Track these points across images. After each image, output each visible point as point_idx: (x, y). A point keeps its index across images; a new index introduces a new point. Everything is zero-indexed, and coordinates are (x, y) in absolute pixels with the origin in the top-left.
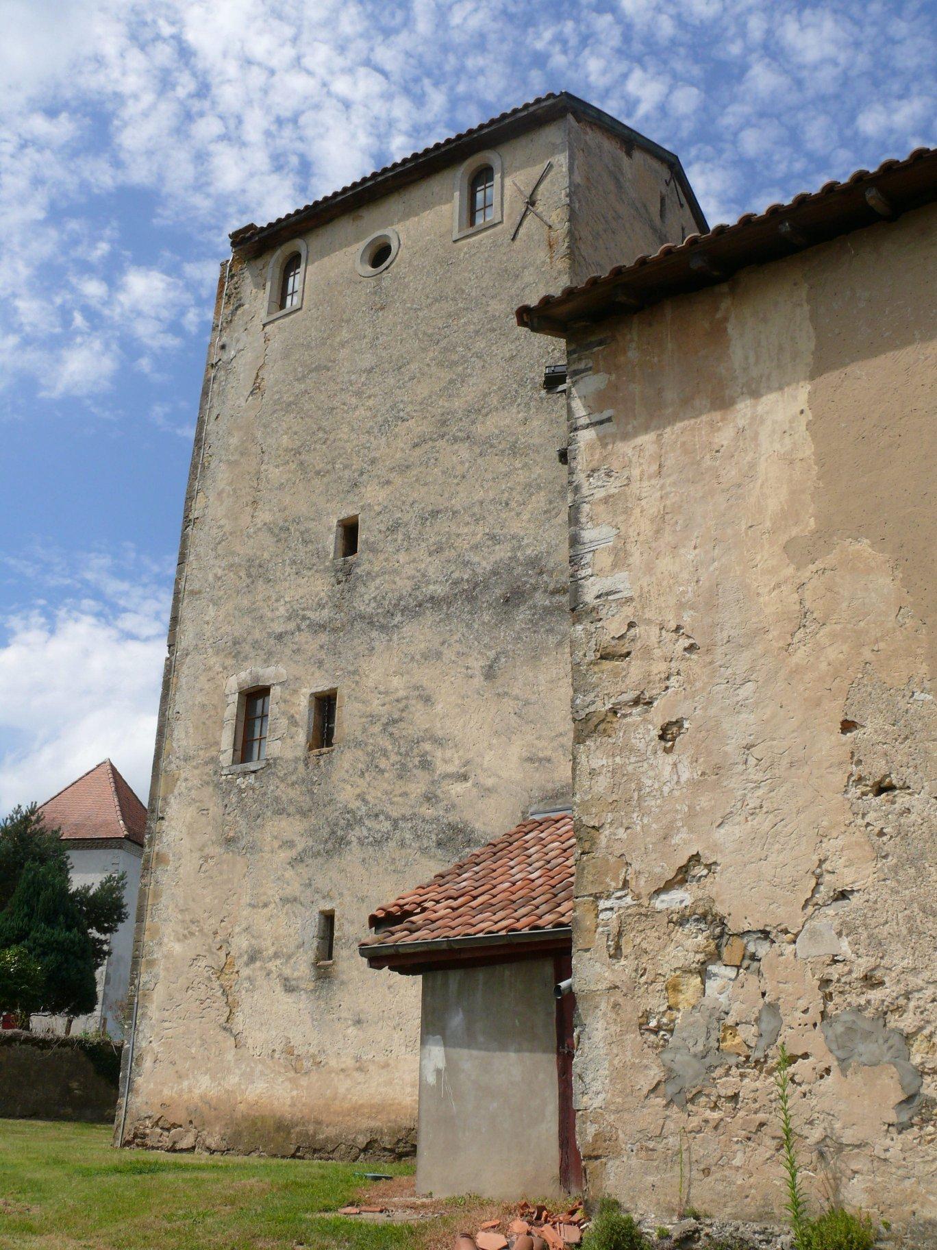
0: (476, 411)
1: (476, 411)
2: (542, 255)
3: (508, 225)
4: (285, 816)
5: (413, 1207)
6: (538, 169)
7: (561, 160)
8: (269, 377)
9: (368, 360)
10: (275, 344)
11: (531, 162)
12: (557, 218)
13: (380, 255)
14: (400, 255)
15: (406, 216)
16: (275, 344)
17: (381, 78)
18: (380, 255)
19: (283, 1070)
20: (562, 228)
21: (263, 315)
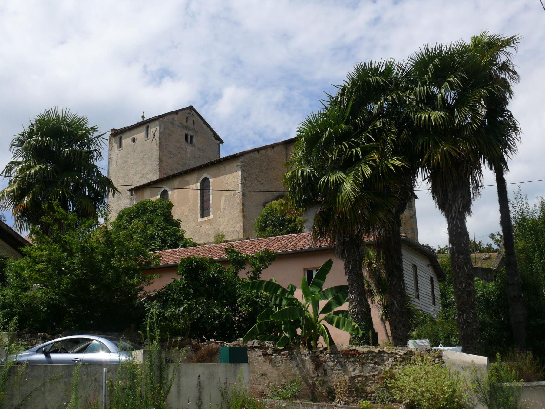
0: (147, 173)
1: (147, 173)
2: (155, 146)
3: (151, 139)
4: (226, 391)
5: (456, 151)
6: (155, 129)
7: (158, 128)
8: (119, 162)
9: (133, 162)
10: (119, 156)
11: (154, 127)
12: (158, 139)
13: (134, 140)
14: (137, 141)
15: (138, 133)
16: (119, 156)
17: (170, 374)
18: (134, 140)
19: (322, 342)
20: (158, 141)
21: (116, 150)
